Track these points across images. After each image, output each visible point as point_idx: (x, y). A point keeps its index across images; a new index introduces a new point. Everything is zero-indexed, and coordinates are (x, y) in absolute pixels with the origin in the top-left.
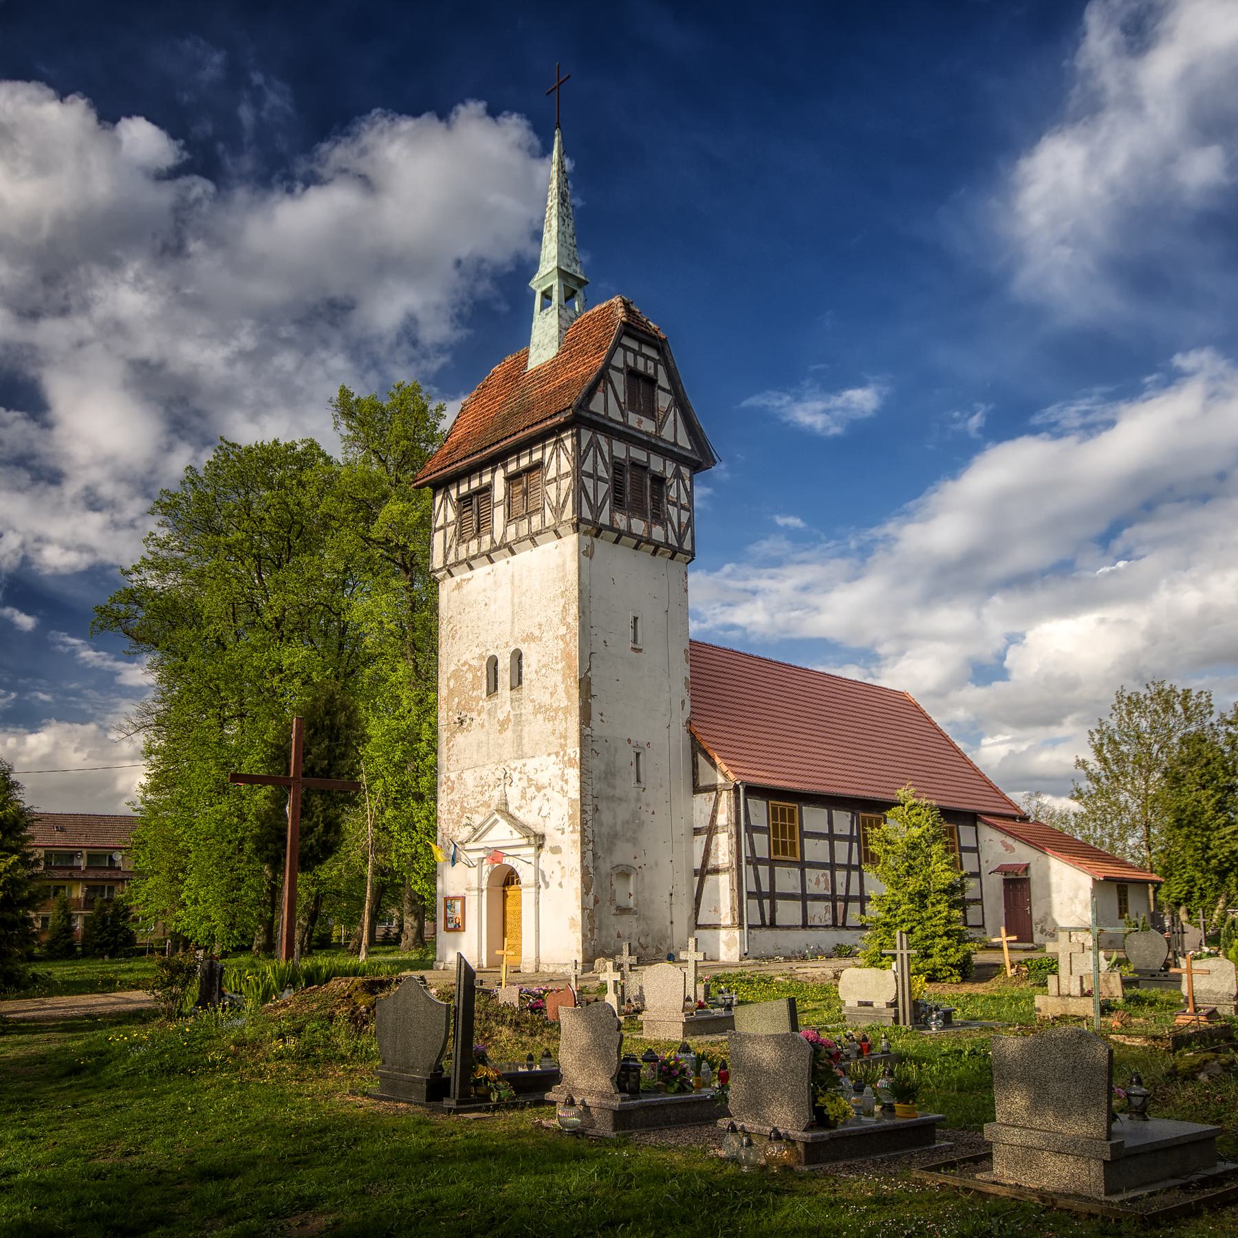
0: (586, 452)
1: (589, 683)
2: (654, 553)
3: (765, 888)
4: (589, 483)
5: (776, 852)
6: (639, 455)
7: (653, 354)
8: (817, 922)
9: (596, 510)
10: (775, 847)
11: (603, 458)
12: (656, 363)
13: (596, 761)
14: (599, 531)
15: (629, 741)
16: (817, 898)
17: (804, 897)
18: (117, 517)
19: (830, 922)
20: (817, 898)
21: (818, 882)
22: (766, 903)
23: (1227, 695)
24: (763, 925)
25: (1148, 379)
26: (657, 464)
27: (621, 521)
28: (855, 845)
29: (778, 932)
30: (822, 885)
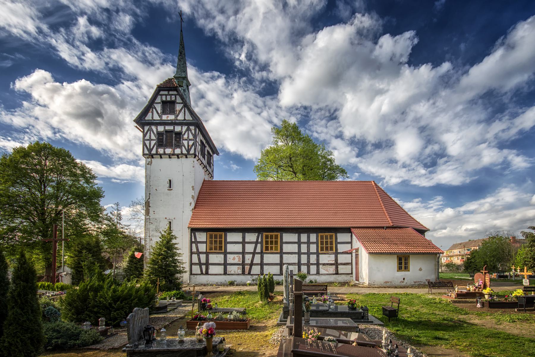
0: (147, 133)
1: (149, 203)
4: (147, 143)
6: (170, 128)
7: (175, 93)
8: (232, 272)
9: (150, 150)
11: (153, 133)
12: (175, 95)
13: (151, 226)
15: (166, 218)
18: (410, 168)
25: (11, 87)
26: (178, 129)
27: (161, 151)
29: (210, 276)
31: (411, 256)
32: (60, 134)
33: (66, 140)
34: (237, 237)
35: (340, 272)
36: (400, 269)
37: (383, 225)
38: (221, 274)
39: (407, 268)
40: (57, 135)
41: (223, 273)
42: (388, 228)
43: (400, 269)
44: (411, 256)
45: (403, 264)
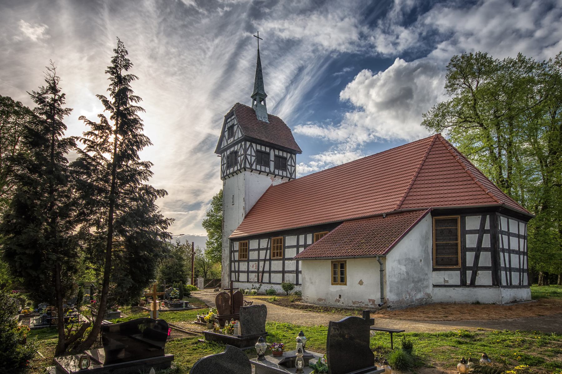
2: (267, 175)
3: (508, 266)
5: (274, 256)
8: (252, 281)
10: (240, 256)
14: (276, 176)
16: (253, 272)
17: (248, 272)
19: (256, 281)
20: (253, 272)
21: (253, 267)
22: (237, 274)
23: (161, 1)
24: (236, 281)
27: (277, 172)
28: (268, 251)
29: (239, 283)
30: (255, 267)
31: (348, 261)
32: (374, 134)
33: (379, 138)
34: (473, 223)
35: (272, 281)
36: (335, 281)
37: (380, 212)
38: (490, 286)
39: (343, 281)
40: (371, 136)
41: (459, 283)
42: (388, 215)
43: (335, 281)
44: (348, 261)
45: (339, 273)
